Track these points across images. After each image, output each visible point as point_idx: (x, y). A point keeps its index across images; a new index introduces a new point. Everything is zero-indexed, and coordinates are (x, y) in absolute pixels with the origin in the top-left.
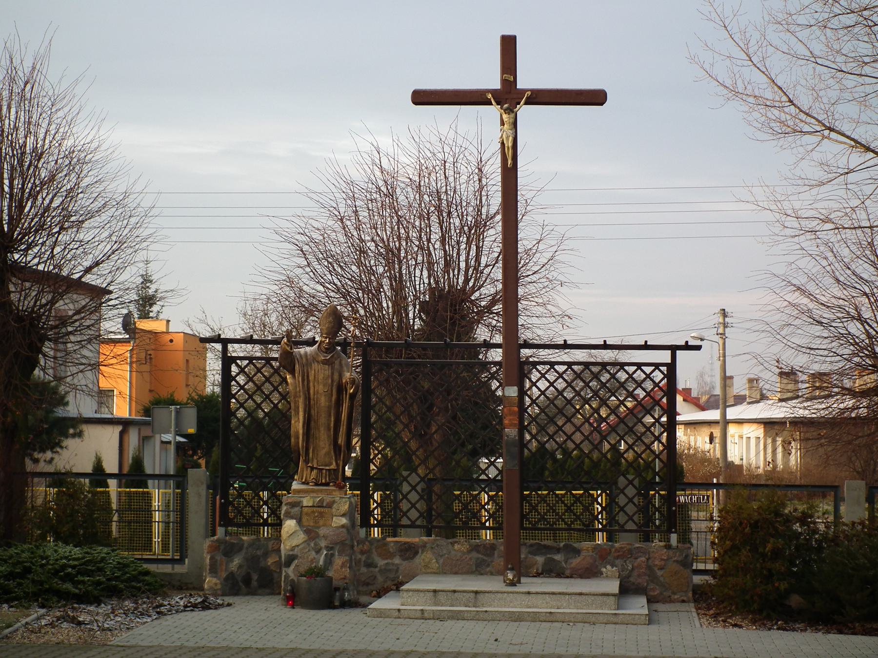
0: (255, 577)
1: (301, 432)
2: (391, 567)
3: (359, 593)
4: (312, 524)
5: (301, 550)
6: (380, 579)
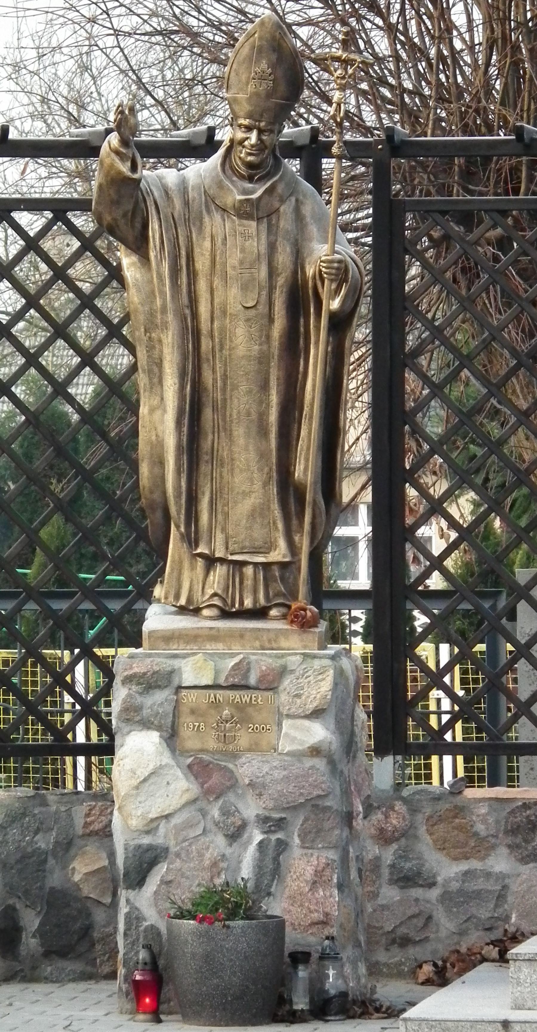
0: (31, 921)
1: (170, 442)
2: (480, 884)
3: (375, 970)
4: (212, 744)
5: (179, 829)
6: (446, 924)
